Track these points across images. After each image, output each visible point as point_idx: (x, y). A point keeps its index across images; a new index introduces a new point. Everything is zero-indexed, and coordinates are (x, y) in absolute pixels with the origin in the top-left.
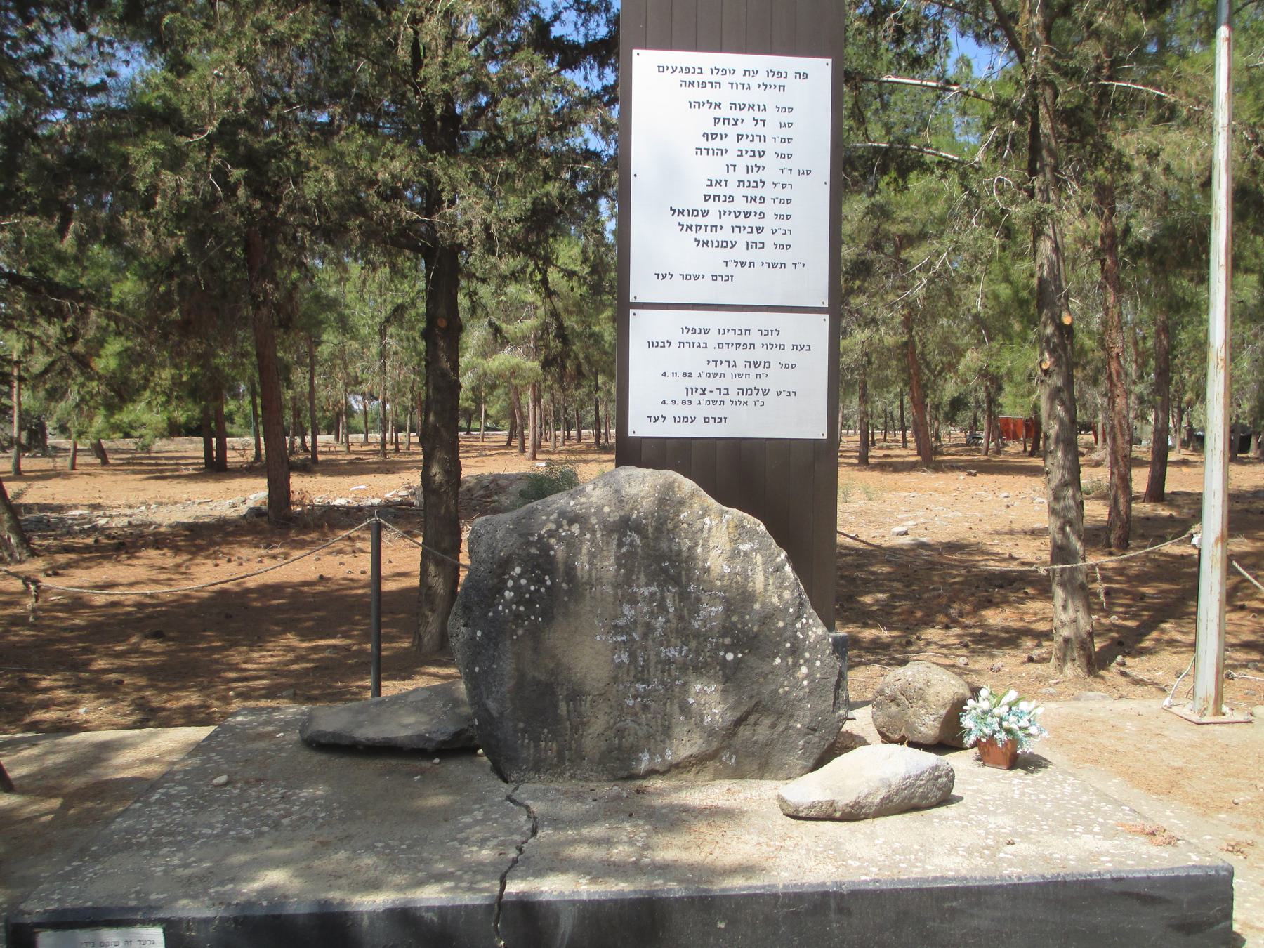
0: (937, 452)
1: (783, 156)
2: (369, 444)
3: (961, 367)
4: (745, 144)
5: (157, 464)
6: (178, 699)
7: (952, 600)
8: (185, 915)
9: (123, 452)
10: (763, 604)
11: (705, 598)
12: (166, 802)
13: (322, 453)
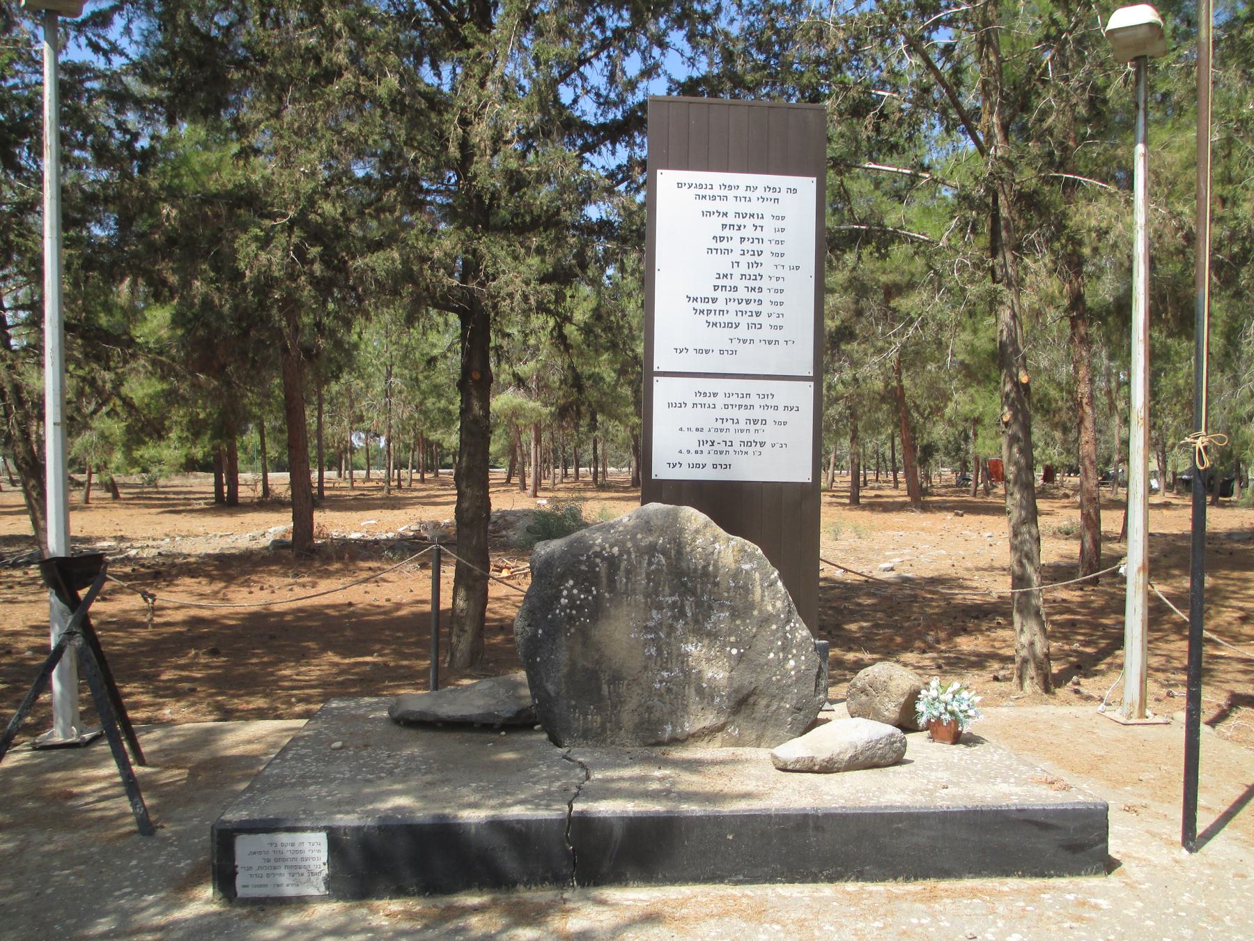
0: (925, 492)
1: (777, 255)
2: (372, 480)
3: (948, 411)
4: (747, 245)
5: (166, 499)
6: (248, 702)
7: (929, 628)
8: (342, 824)
9: (131, 486)
10: (760, 611)
11: (715, 605)
12: (300, 758)
13: (329, 489)
